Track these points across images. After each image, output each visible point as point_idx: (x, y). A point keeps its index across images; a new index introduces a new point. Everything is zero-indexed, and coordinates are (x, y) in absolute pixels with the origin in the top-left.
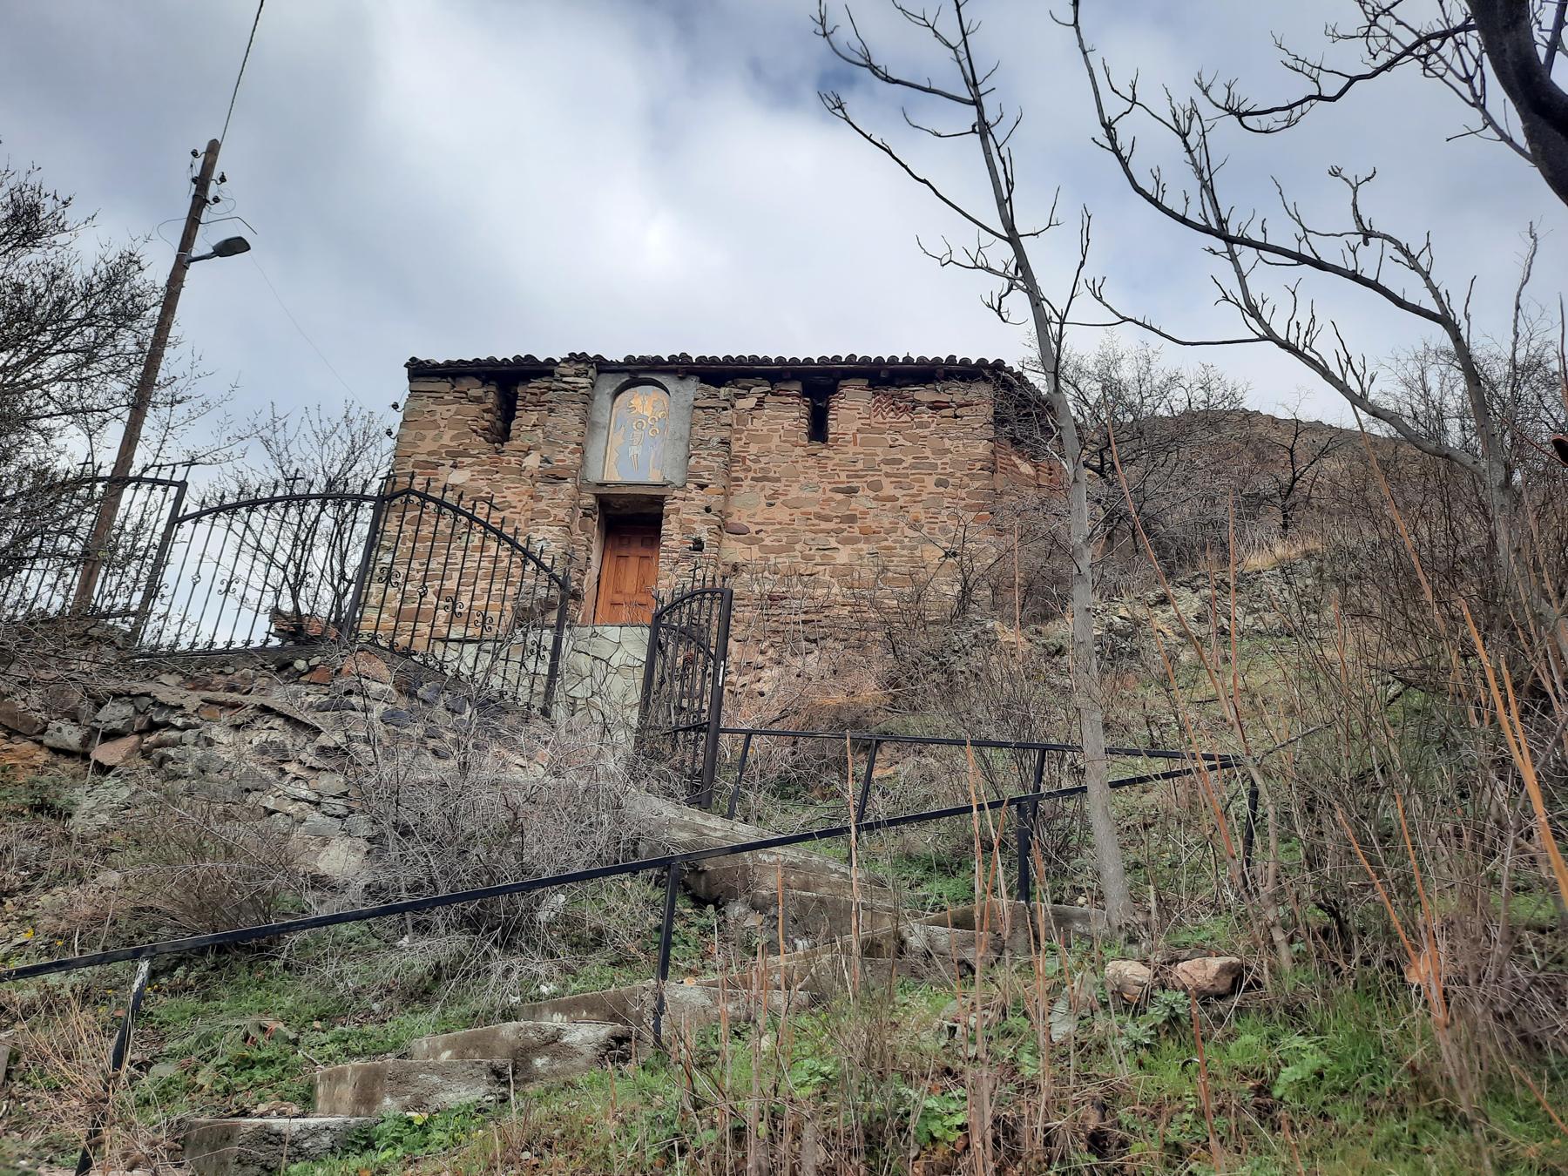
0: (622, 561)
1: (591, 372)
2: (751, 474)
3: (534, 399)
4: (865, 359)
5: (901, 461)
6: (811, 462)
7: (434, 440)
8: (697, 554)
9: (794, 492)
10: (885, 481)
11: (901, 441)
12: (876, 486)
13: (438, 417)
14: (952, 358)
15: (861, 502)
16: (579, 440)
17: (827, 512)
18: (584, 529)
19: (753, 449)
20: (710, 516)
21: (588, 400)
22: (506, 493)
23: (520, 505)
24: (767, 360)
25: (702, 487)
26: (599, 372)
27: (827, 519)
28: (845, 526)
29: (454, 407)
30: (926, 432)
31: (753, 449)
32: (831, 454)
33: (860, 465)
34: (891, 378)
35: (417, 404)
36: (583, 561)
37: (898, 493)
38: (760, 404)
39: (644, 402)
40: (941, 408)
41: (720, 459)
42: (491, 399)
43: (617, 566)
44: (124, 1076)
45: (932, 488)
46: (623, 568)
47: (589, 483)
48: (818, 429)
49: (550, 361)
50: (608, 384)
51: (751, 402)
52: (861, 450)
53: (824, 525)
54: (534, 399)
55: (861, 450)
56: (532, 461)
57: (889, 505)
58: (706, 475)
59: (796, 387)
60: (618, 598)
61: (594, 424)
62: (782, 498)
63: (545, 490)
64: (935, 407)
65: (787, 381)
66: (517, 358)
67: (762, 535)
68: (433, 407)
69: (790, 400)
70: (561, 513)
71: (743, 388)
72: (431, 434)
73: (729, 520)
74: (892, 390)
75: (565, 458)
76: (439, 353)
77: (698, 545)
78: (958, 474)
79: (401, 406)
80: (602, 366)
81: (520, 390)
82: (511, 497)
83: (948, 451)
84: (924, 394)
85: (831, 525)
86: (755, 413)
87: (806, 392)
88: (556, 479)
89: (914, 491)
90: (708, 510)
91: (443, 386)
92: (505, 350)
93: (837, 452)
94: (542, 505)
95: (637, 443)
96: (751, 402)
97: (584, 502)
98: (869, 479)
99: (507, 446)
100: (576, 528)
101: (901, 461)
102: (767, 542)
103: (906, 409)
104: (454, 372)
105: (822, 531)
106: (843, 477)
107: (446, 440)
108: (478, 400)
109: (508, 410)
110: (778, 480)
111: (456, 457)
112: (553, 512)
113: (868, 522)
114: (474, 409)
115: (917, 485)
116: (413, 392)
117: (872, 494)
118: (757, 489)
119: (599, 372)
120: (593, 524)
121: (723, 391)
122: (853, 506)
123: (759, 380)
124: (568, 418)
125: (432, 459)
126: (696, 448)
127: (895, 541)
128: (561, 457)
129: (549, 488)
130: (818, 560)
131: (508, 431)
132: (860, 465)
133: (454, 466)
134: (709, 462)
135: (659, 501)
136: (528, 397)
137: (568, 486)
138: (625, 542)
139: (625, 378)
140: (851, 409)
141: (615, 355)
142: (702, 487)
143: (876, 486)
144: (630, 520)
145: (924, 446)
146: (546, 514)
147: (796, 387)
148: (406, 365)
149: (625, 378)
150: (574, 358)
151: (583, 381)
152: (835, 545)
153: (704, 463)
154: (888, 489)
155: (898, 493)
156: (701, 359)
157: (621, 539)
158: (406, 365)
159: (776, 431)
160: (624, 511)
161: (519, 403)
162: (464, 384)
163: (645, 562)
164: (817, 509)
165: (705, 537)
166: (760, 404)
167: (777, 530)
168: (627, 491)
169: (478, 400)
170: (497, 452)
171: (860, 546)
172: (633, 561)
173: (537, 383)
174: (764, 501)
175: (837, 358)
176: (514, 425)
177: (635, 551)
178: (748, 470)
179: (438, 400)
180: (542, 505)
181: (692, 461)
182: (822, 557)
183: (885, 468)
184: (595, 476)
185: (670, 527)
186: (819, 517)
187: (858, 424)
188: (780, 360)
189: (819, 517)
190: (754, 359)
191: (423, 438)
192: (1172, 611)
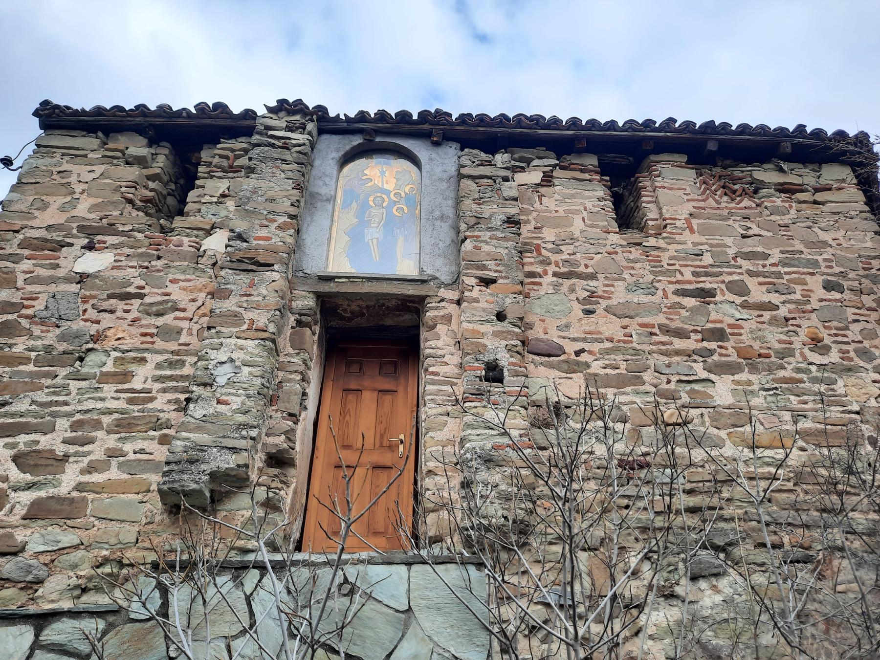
0: (351, 397)
1: (310, 126)
2: (551, 269)
3: (225, 163)
4: (688, 125)
5: (767, 256)
6: (636, 253)
7: (62, 209)
8: (496, 388)
9: (620, 294)
10: (751, 283)
11: (755, 230)
12: (740, 289)
13: (73, 179)
14: (801, 128)
15: (725, 311)
16: (293, 211)
17: (677, 324)
18: (298, 345)
19: (549, 234)
20: (505, 326)
21: (305, 161)
22: (171, 288)
23: (192, 307)
24: (555, 122)
25: (487, 282)
26: (321, 132)
27: (681, 334)
28: (713, 345)
29: (99, 169)
30: (786, 219)
31: (549, 234)
32: (661, 243)
33: (707, 259)
34: (725, 153)
35: (43, 163)
36: (297, 399)
37: (776, 299)
38: (547, 180)
39: (382, 174)
40: (793, 192)
41: (510, 244)
42: (161, 161)
43: (344, 405)
44: (59, 565)
45: (822, 293)
46: (351, 406)
47: (307, 276)
48: (627, 215)
49: (249, 114)
50: (332, 148)
51: (534, 176)
52: (703, 239)
53: (679, 344)
54: (225, 163)
55: (703, 239)
56: (217, 243)
57: (767, 315)
58: (491, 264)
59: (592, 161)
60: (348, 457)
61: (314, 196)
62: (604, 303)
63: (237, 281)
64: (785, 189)
65: (580, 152)
66: (201, 108)
67: (584, 357)
68: (65, 166)
69: (587, 176)
70: (262, 319)
71: (521, 160)
72: (57, 201)
73: (531, 334)
74: (717, 170)
75: (270, 236)
76: (81, 99)
77: (494, 373)
78: (852, 275)
79: (16, 164)
80: (325, 123)
81: (205, 155)
82: (177, 294)
83: (825, 244)
84: (767, 175)
85: (690, 344)
86: (543, 190)
87: (604, 169)
88: (251, 264)
89: (798, 296)
90: (501, 316)
91: (89, 143)
92: (185, 98)
93: (671, 241)
94: (229, 305)
95: (375, 229)
96: (534, 176)
97: (298, 304)
98: (728, 279)
99: (178, 222)
100: (284, 342)
101: (767, 256)
102: (596, 367)
103: (744, 193)
104: (105, 123)
105: (678, 353)
106: (688, 275)
107: (83, 209)
108: (141, 161)
109: (185, 178)
110: (592, 277)
111: (92, 237)
112: (247, 315)
113: (746, 338)
114: (133, 173)
115: (798, 288)
116: (41, 147)
117: (739, 300)
118: (565, 289)
119: (321, 132)
120: (312, 338)
121: (501, 158)
122: (713, 316)
123: (541, 151)
124: (274, 183)
125: (56, 236)
126: (470, 227)
127: (798, 370)
128: (264, 233)
129: (245, 278)
130: (685, 399)
131: (183, 202)
132: (707, 259)
133: (90, 247)
134: (491, 247)
135: (413, 306)
136: (216, 160)
137: (276, 277)
138: (355, 368)
139: (357, 140)
140: (672, 190)
141: (341, 107)
142: (487, 282)
143: (740, 289)
144: (368, 335)
145: (791, 238)
146: (235, 318)
147: (592, 161)
148: (36, 114)
149: (357, 140)
150: (283, 107)
151: (298, 137)
152: (704, 375)
153: (486, 248)
154: (758, 293)
155: (776, 299)
156: (464, 118)
157: (349, 364)
158: (36, 114)
159: (577, 212)
160: (358, 321)
161: (201, 169)
162: (122, 141)
163: (388, 398)
164: (661, 319)
165: (505, 360)
166: (547, 180)
167: (608, 352)
168: (367, 288)
169: (141, 161)
170: (163, 230)
171: (744, 376)
172: (368, 397)
173: (227, 145)
174: (578, 309)
175: (649, 124)
176: (192, 195)
177: (372, 380)
178: (546, 262)
179: (78, 156)
180: (229, 305)
181: (468, 245)
182: (691, 393)
183: (746, 265)
184: (314, 265)
185: (438, 344)
186: (665, 330)
187: (689, 207)
188: (574, 122)
189: (665, 330)
190: (537, 120)
191: (45, 207)
192: (187, 364)
